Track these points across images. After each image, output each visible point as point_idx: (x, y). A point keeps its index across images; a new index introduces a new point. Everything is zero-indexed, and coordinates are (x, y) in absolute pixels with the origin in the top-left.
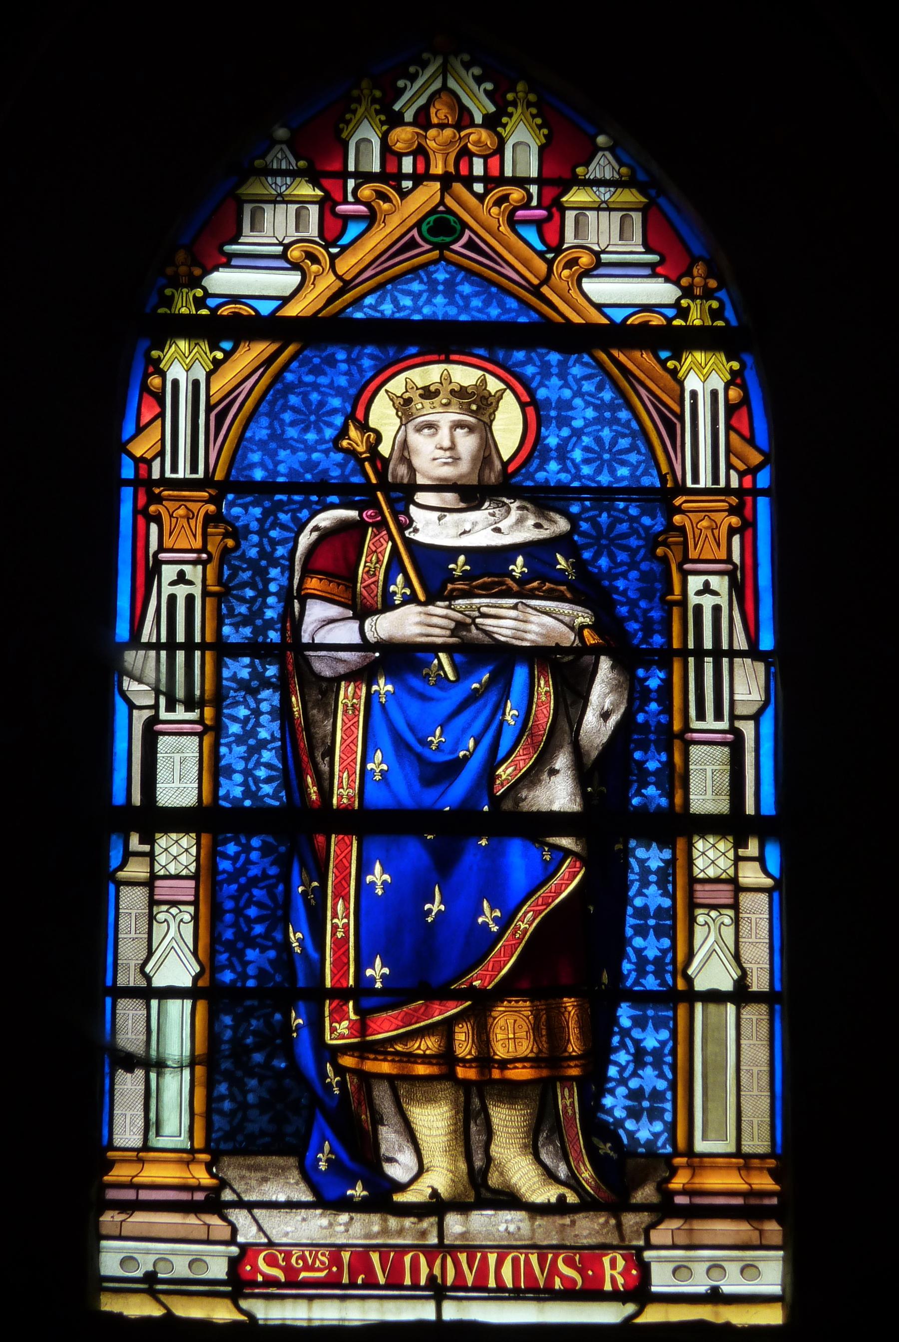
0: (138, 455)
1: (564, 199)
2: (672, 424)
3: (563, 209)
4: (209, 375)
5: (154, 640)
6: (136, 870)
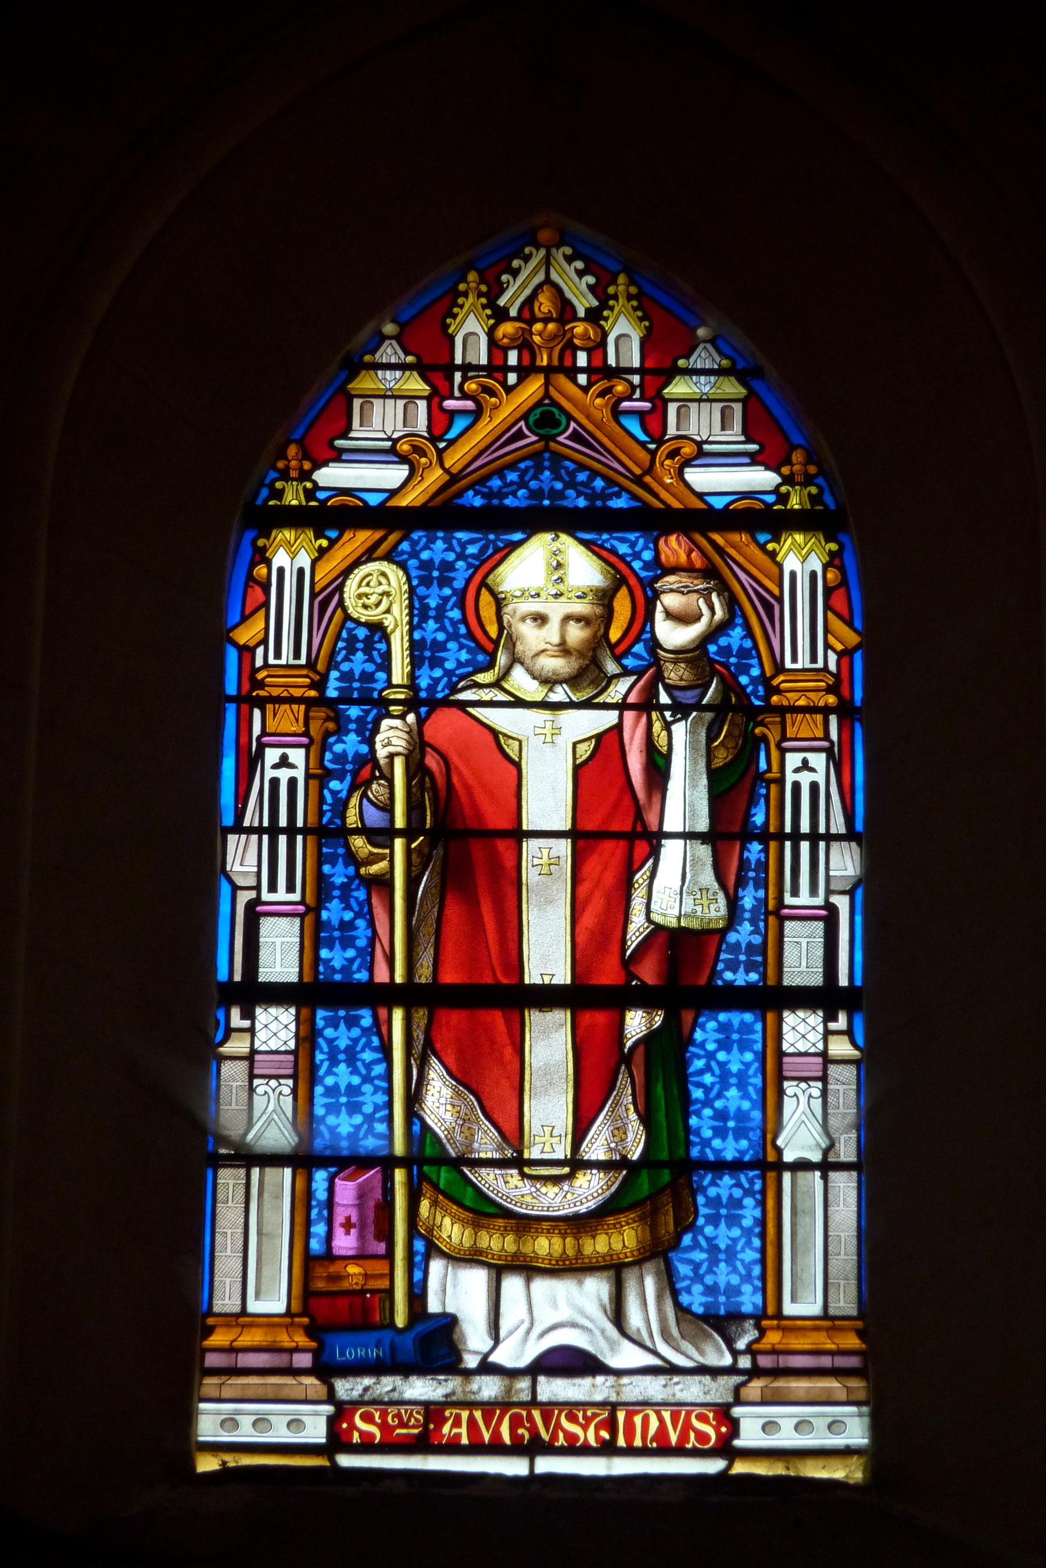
0: (242, 643)
1: (665, 391)
2: (770, 607)
3: (666, 402)
4: (314, 563)
5: (256, 824)
6: (237, 1046)
